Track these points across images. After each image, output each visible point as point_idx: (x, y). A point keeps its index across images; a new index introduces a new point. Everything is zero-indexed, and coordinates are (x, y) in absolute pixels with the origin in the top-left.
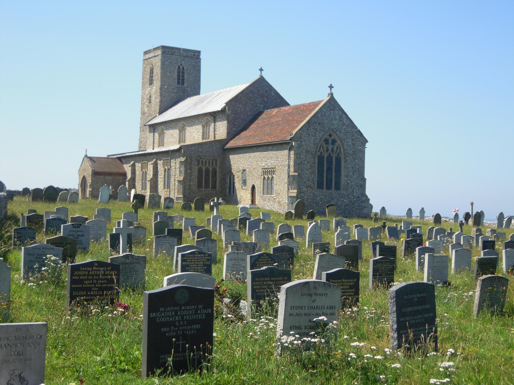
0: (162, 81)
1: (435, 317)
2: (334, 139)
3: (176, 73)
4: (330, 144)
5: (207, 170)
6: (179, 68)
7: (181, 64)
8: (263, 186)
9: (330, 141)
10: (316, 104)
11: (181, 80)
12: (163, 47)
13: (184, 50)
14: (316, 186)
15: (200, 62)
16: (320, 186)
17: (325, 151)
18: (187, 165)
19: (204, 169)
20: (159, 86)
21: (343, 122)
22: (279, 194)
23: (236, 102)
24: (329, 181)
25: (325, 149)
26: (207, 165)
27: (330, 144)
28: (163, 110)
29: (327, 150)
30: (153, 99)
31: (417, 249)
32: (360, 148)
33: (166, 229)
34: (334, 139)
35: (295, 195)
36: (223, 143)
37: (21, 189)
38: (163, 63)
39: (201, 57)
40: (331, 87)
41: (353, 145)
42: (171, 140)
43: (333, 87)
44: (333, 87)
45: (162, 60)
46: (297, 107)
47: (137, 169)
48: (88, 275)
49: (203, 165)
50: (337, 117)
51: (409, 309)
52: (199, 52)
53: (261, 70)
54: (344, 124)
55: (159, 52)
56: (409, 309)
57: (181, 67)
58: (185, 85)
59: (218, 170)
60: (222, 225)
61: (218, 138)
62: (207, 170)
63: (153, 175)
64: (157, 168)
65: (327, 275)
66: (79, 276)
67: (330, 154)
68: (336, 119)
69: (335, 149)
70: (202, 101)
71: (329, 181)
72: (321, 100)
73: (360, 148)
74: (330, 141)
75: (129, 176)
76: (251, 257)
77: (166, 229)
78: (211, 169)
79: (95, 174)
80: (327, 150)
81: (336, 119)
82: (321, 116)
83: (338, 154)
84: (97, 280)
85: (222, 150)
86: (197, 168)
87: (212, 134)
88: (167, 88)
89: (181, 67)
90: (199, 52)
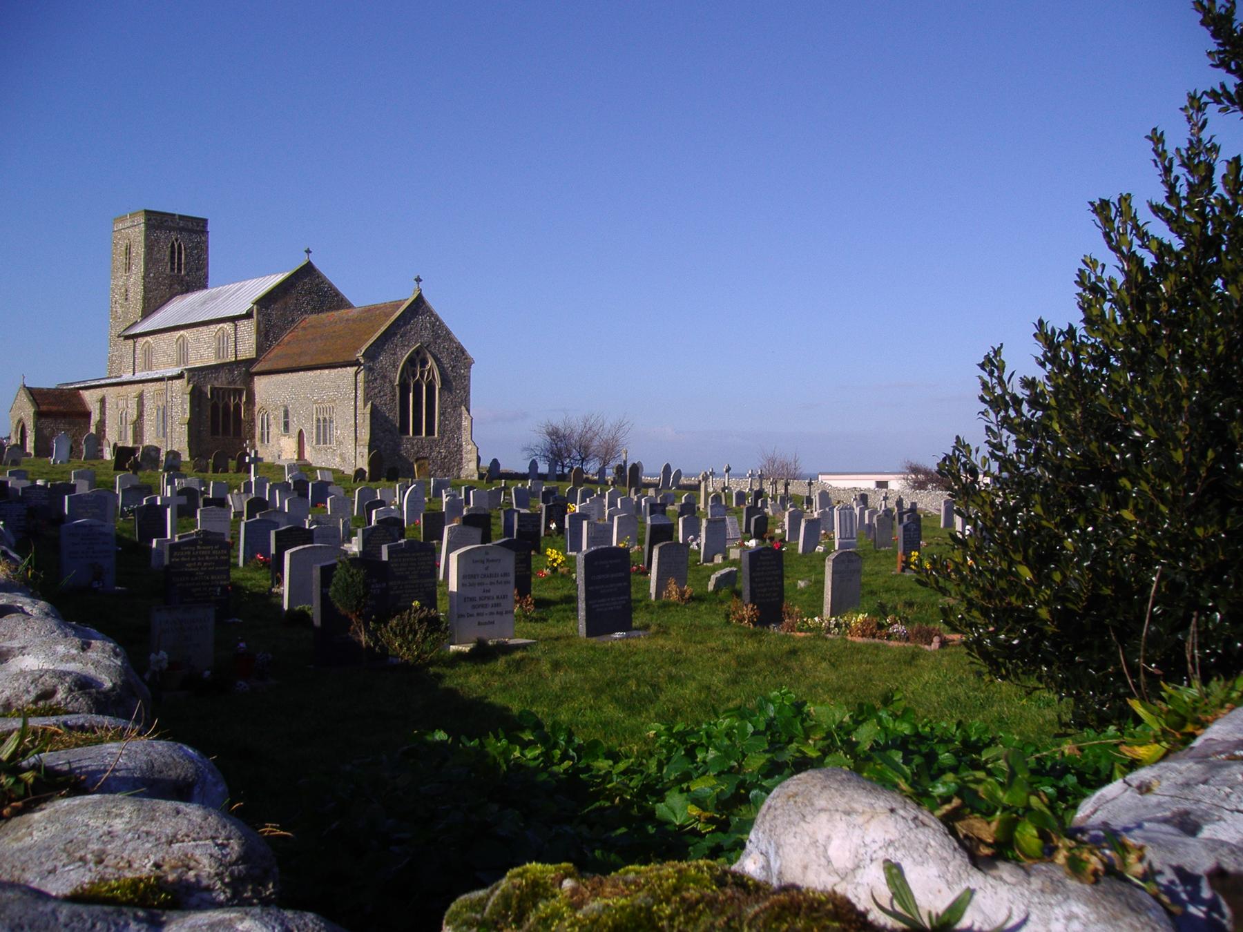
0: (146, 264)
1: (629, 586)
6: (173, 245)
10: (397, 305)
13: (182, 217)
18: (196, 396)
20: (141, 274)
22: (341, 443)
28: (147, 313)
30: (131, 294)
35: (539, 471)
36: (250, 362)
42: (164, 360)
46: (369, 310)
47: (146, 428)
48: (192, 556)
51: (599, 577)
52: (205, 221)
53: (418, 280)
56: (599, 577)
60: (441, 577)
64: (142, 405)
65: (322, 568)
66: (180, 557)
70: (213, 298)
72: (402, 298)
75: (95, 417)
76: (277, 534)
79: (39, 415)
84: (203, 562)
85: (246, 370)
87: (231, 350)
90: (205, 221)
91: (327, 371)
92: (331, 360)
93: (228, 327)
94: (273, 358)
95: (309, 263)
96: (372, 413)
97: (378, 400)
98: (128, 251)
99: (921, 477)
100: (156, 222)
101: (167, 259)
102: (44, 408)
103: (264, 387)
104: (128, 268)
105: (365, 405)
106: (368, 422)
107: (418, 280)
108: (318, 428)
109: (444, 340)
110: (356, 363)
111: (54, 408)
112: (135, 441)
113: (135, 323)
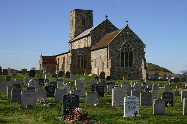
2: (129, 45)
3: (82, 20)
4: (127, 47)
5: (82, 60)
6: (83, 18)
7: (84, 17)
8: (101, 67)
9: (127, 46)
11: (84, 22)
12: (76, 10)
14: (120, 66)
15: (92, 15)
16: (122, 65)
17: (124, 50)
19: (81, 59)
21: (133, 37)
23: (95, 31)
24: (127, 63)
25: (124, 49)
26: (82, 58)
27: (127, 47)
29: (126, 50)
31: (125, 98)
32: (142, 48)
34: (129, 45)
37: (20, 69)
38: (76, 16)
39: (93, 13)
40: (127, 22)
41: (138, 47)
43: (128, 22)
44: (128, 22)
45: (75, 15)
49: (83, 58)
50: (130, 35)
53: (107, 16)
54: (133, 38)
55: (74, 12)
57: (84, 18)
58: (86, 25)
59: (87, 60)
61: (88, 46)
62: (82, 60)
63: (63, 63)
67: (127, 51)
68: (129, 36)
69: (129, 49)
71: (127, 63)
73: (142, 48)
74: (127, 46)
78: (84, 59)
80: (126, 50)
81: (129, 36)
82: (122, 35)
83: (131, 51)
85: (88, 50)
86: (77, 59)
88: (78, 27)
89: (84, 18)
91: (103, 49)
92: (102, 46)
93: (86, 38)
94: (97, 45)
95: (107, 19)
96: (112, 61)
97: (114, 57)
98: (72, 20)
99: (74, 96)
100: (78, 12)
101: (81, 22)
102: (45, 61)
103: (93, 54)
104: (72, 25)
105: (110, 59)
106: (110, 63)
107: (127, 22)
108: (101, 65)
109: (136, 39)
110: (107, 47)
111: (48, 61)
112: (62, 70)
113: (73, 39)
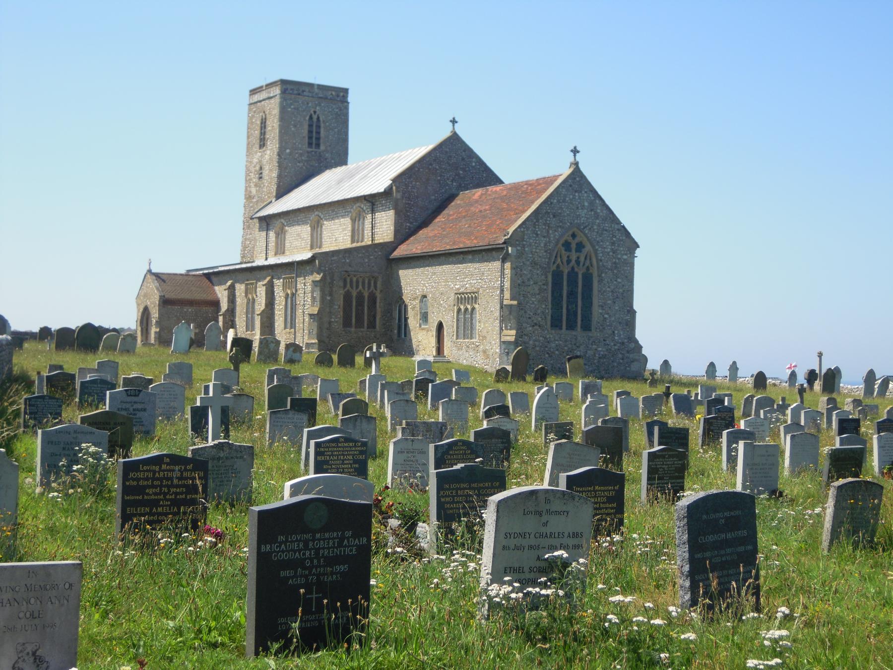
0: (281, 140)
1: (755, 551)
2: (581, 242)
3: (306, 127)
4: (573, 251)
5: (360, 297)
6: (311, 118)
7: (315, 112)
8: (457, 324)
9: (574, 246)
10: (549, 181)
11: (314, 138)
12: (284, 83)
13: (320, 87)
14: (549, 323)
15: (347, 108)
16: (556, 323)
17: (565, 263)
18: (325, 287)
19: (354, 294)
20: (276, 150)
21: (596, 213)
22: (484, 337)
23: (410, 178)
24: (572, 315)
25: (565, 259)
26: (360, 287)
27: (573, 251)
28: (282, 191)
29: (569, 261)
30: (266, 172)
31: (725, 433)
32: (625, 257)
33: (289, 399)
34: (581, 242)
36: (387, 248)
37: (36, 329)
38: (283, 110)
39: (350, 99)
40: (575, 151)
41: (614, 252)
42: (297, 243)
43: (578, 152)
44: (578, 152)
45: (281, 104)
46: (516, 187)
47: (237, 294)
48: (154, 479)
49: (352, 287)
50: (586, 204)
51: (711, 538)
52: (346, 91)
53: (454, 121)
54: (597, 216)
55: (277, 91)
56: (711, 538)
57: (315, 117)
58: (322, 148)
59: (378, 295)
60: (386, 392)
61: (379, 240)
62: (360, 297)
63: (266, 305)
64: (273, 292)
66: (138, 480)
67: (573, 268)
68: (583, 207)
69: (582, 259)
70: (351, 176)
71: (572, 315)
72: (557, 173)
73: (625, 257)
74: (574, 246)
75: (224, 306)
77: (289, 399)
78: (366, 295)
79: (165, 302)
80: (569, 261)
81: (583, 207)
82: (558, 201)
83: (588, 269)
84: (168, 487)
85: (386, 262)
86: (342, 292)
87: (367, 233)
88: (290, 154)
89: (315, 117)
90: (346, 91)
